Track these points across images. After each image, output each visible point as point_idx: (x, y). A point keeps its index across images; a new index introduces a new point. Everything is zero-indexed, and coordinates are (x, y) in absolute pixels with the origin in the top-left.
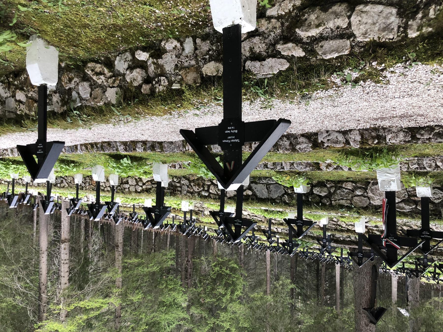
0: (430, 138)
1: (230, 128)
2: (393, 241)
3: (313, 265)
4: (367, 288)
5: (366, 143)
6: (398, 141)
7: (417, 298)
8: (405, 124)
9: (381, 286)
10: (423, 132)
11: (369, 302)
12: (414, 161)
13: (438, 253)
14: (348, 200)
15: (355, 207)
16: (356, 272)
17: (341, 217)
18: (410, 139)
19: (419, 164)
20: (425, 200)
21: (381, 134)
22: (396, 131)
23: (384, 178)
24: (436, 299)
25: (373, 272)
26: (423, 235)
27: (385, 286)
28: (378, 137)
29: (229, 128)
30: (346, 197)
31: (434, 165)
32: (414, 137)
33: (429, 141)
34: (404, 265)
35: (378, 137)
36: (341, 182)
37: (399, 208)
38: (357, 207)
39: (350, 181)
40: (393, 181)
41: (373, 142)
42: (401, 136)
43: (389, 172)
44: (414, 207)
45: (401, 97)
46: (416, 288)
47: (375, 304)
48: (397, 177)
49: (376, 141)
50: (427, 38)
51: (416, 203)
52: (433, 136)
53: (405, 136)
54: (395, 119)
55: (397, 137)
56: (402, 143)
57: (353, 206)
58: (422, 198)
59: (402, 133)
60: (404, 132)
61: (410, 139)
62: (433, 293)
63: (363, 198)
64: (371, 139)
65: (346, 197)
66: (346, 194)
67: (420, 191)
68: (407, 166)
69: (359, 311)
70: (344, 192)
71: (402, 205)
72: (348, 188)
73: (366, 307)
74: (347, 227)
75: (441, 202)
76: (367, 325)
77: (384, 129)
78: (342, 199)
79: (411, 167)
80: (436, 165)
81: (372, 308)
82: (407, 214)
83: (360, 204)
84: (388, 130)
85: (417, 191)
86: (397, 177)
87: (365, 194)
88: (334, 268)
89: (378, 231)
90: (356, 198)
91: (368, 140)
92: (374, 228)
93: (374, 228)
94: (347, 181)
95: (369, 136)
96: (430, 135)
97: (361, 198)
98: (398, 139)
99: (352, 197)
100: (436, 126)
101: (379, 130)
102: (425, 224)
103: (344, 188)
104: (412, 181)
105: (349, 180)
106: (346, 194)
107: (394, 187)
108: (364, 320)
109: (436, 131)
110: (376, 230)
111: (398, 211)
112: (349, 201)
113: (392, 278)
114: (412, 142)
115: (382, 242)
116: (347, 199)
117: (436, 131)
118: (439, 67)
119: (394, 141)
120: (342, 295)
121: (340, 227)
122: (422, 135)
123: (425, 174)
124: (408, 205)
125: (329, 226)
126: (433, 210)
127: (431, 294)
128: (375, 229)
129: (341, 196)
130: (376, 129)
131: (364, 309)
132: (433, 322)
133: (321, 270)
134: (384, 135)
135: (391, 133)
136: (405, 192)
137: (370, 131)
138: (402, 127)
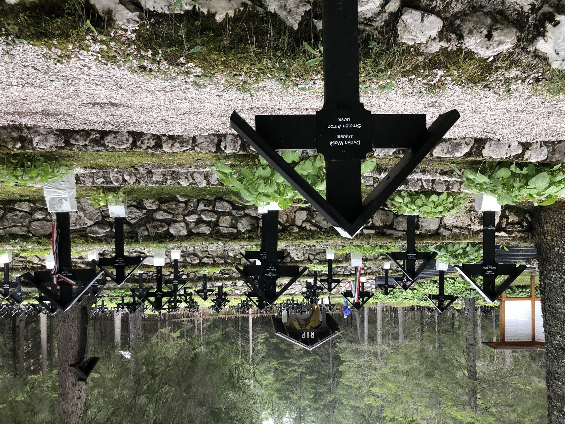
0: (86, 145)
1: (343, 120)
2: (67, 276)
3: (6, 322)
4: (75, 338)
5: (4, 146)
6: (48, 147)
7: (139, 335)
8: (55, 125)
9: (103, 330)
10: (78, 137)
11: (77, 355)
12: (99, 174)
13: (154, 279)
14: (24, 226)
15: (33, 236)
16: (60, 321)
17: (22, 250)
18: (63, 145)
19: (105, 178)
20: (120, 221)
21: (25, 135)
22: (45, 133)
23: (54, 195)
24: (163, 330)
25: (82, 316)
26: (117, 262)
27: (108, 328)
28: (22, 139)
29: (339, 120)
30: (21, 222)
31: (121, 178)
32: (67, 142)
33: (86, 149)
34: (123, 300)
35: (22, 139)
36: (12, 201)
37: (92, 232)
38: (37, 235)
39: (25, 201)
40: (65, 199)
41: (15, 145)
42: (52, 139)
43: (60, 187)
44: (108, 230)
45: (21, 86)
46: (137, 324)
47: (85, 356)
48: (71, 194)
49: (19, 145)
50: (29, 9)
51: (110, 224)
52: (89, 142)
53: (56, 141)
54: (38, 117)
55: (47, 141)
56: (54, 149)
57: (31, 235)
58: (115, 219)
59: (53, 136)
60: (55, 134)
61: (63, 145)
62: (159, 325)
63: (45, 222)
64: (11, 141)
65: (21, 222)
66: (20, 218)
67: (113, 211)
68: (91, 180)
69: (64, 371)
70: (17, 215)
71: (95, 228)
72: (24, 210)
73: (73, 362)
74: (40, 262)
75: (137, 222)
76: (74, 385)
77: (29, 128)
78: (15, 226)
79: (96, 181)
80: (123, 178)
81: (80, 362)
82: (101, 240)
83: (42, 232)
84: (34, 130)
85: (110, 211)
86: (71, 194)
87: (48, 217)
88: (38, 321)
89: (83, 263)
90: (35, 223)
91: (6, 142)
92: (78, 260)
93: (78, 260)
94: (21, 201)
95: (8, 137)
96: (86, 140)
97: (42, 223)
98: (48, 144)
99: (30, 222)
100: (91, 130)
101: (22, 130)
102: (119, 250)
103: (19, 210)
104: (101, 199)
105: (23, 198)
106: (20, 218)
107: (67, 207)
108: (71, 379)
109: (92, 137)
110: (81, 263)
111: (91, 237)
112: (25, 229)
113: (115, 317)
114: (67, 149)
115: (52, 279)
116: (22, 226)
117: (92, 137)
118: (49, 51)
119: (43, 147)
120: (50, 353)
121: (31, 265)
122: (77, 140)
123: (115, 190)
124: (102, 228)
125: (14, 264)
126: (128, 233)
127: (157, 326)
128: (80, 261)
129: (13, 222)
130: (17, 128)
131: (71, 365)
132: (154, 358)
133: (19, 326)
134: (29, 136)
135: (39, 135)
136: (98, 213)
137: (9, 130)
138: (52, 128)
